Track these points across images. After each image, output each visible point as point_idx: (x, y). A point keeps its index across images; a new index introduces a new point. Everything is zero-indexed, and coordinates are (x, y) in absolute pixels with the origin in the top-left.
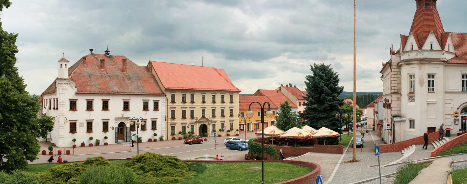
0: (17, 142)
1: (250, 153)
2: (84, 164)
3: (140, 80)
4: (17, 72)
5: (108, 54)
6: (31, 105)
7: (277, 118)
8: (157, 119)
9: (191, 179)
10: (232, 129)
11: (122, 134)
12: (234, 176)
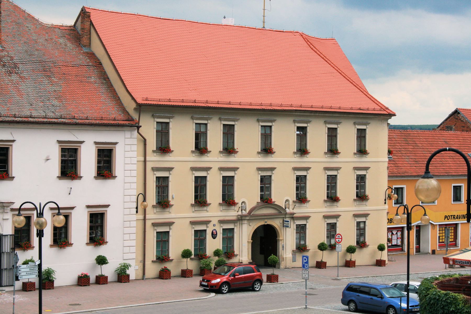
3: (49, 74)
8: (108, 206)
10: (362, 244)
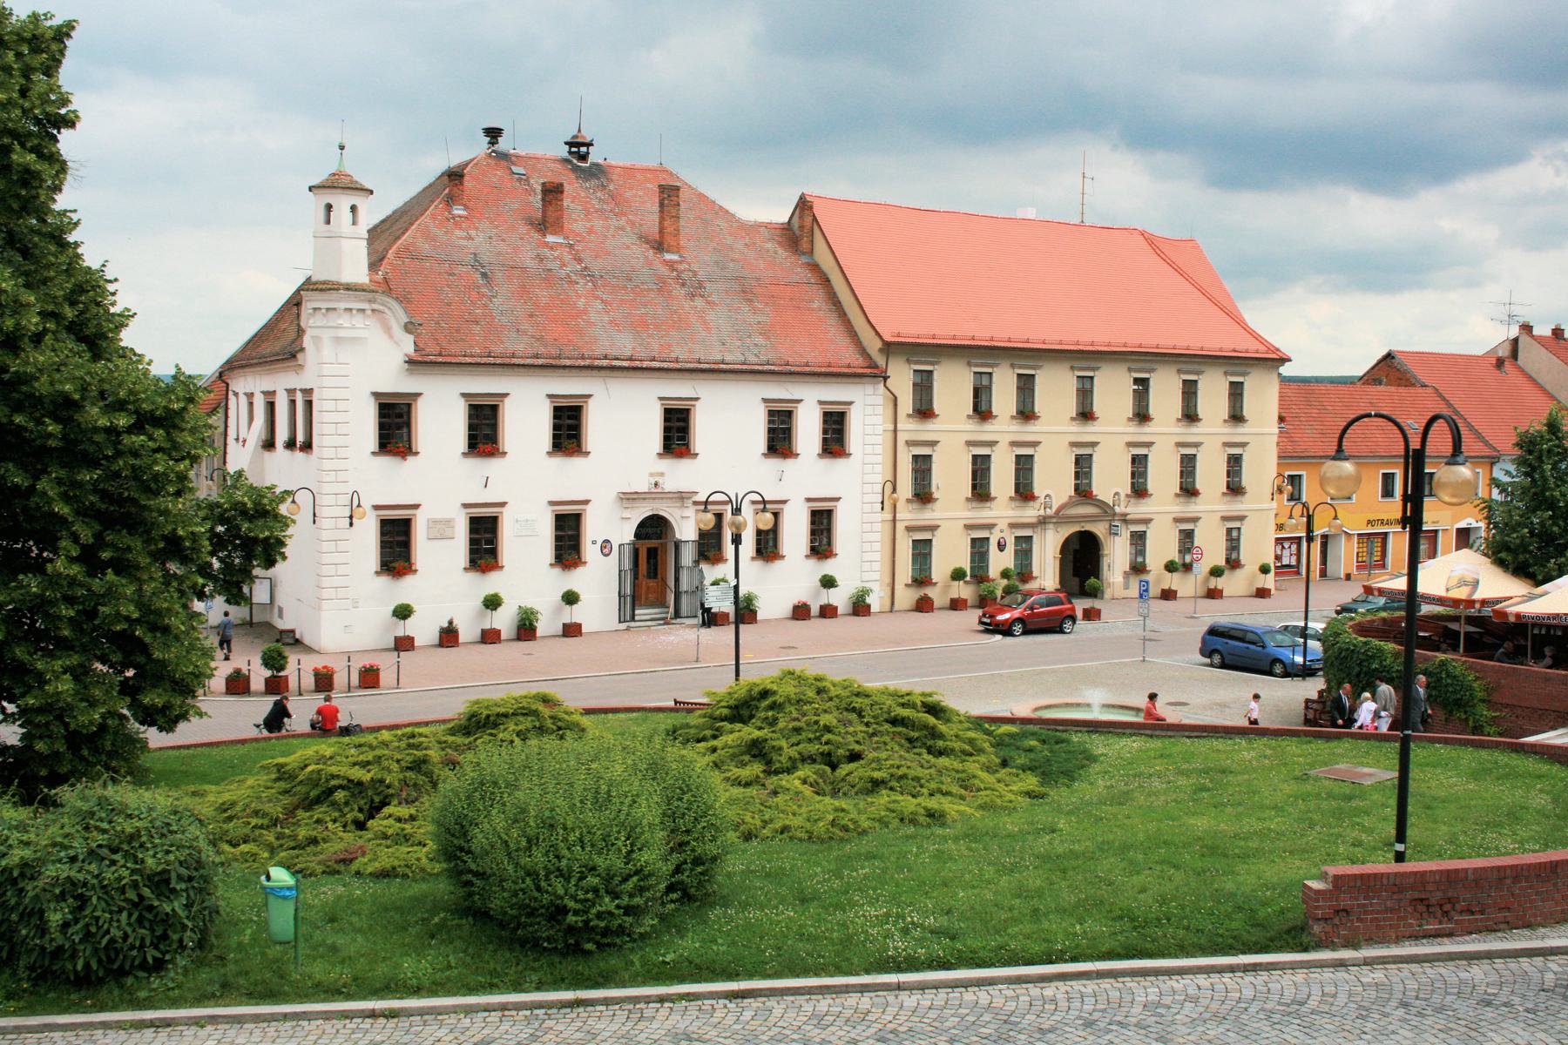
0: (82, 631)
1: (1329, 689)
2: (452, 732)
4: (71, 238)
5: (583, 158)
6: (157, 422)
7: (1490, 508)
9: (1011, 809)
10: (1234, 564)
11: (655, 576)
12: (1240, 804)
